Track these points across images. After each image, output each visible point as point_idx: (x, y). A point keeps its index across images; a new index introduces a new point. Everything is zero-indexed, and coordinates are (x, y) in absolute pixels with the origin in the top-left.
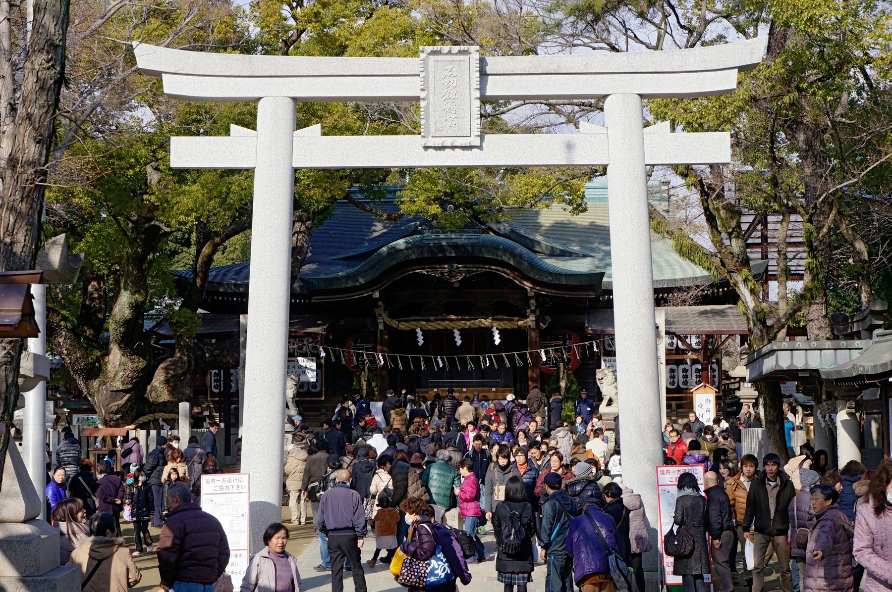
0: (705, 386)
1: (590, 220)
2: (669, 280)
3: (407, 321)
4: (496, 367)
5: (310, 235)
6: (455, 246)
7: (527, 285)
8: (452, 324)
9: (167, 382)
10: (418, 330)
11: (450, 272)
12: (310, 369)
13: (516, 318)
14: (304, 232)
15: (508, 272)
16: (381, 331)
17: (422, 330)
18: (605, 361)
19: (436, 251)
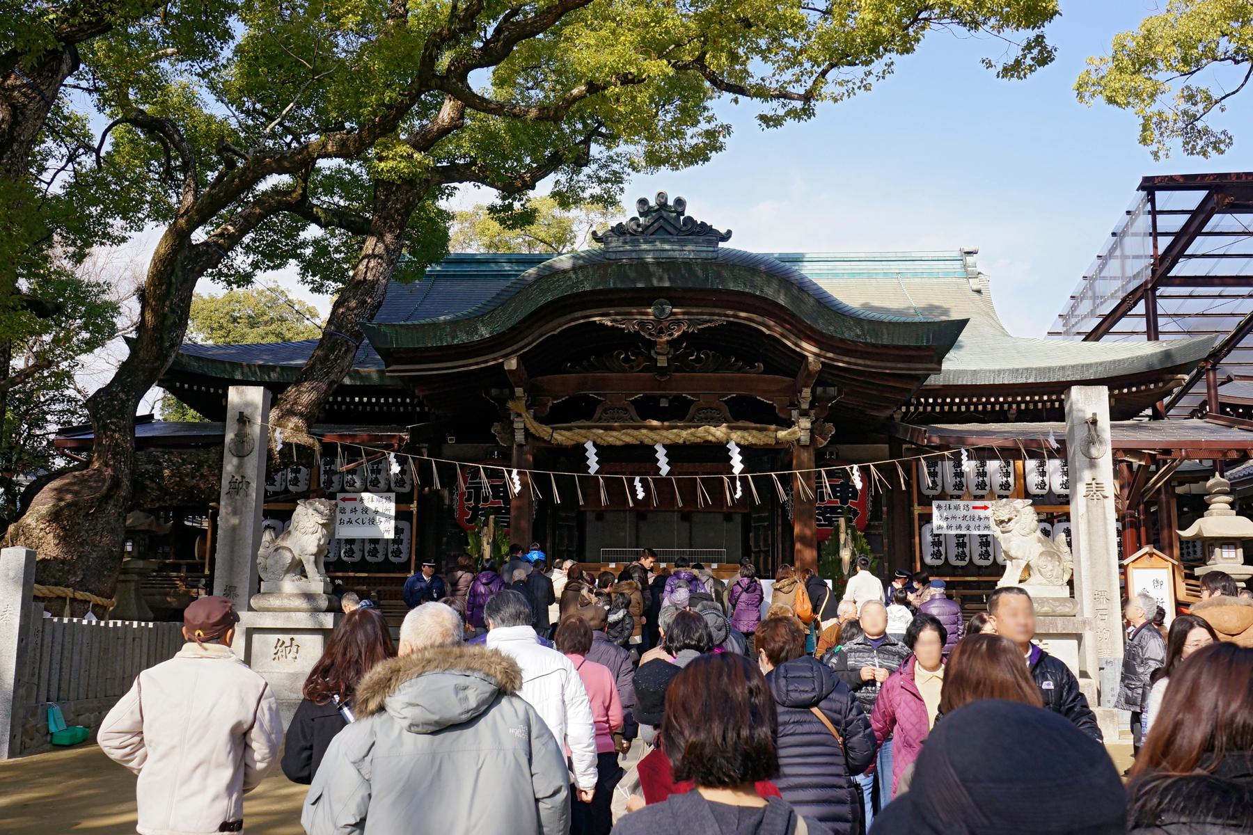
0: (1151, 555)
1: (863, 301)
2: (1040, 371)
3: (569, 429)
4: (758, 501)
5: (391, 262)
6: (668, 265)
7: (809, 349)
8: (652, 434)
9: (55, 517)
10: (589, 445)
11: (659, 321)
12: (383, 515)
13: (773, 427)
14: (380, 257)
15: (772, 323)
16: (520, 446)
17: (595, 445)
18: (939, 507)
19: (632, 275)
